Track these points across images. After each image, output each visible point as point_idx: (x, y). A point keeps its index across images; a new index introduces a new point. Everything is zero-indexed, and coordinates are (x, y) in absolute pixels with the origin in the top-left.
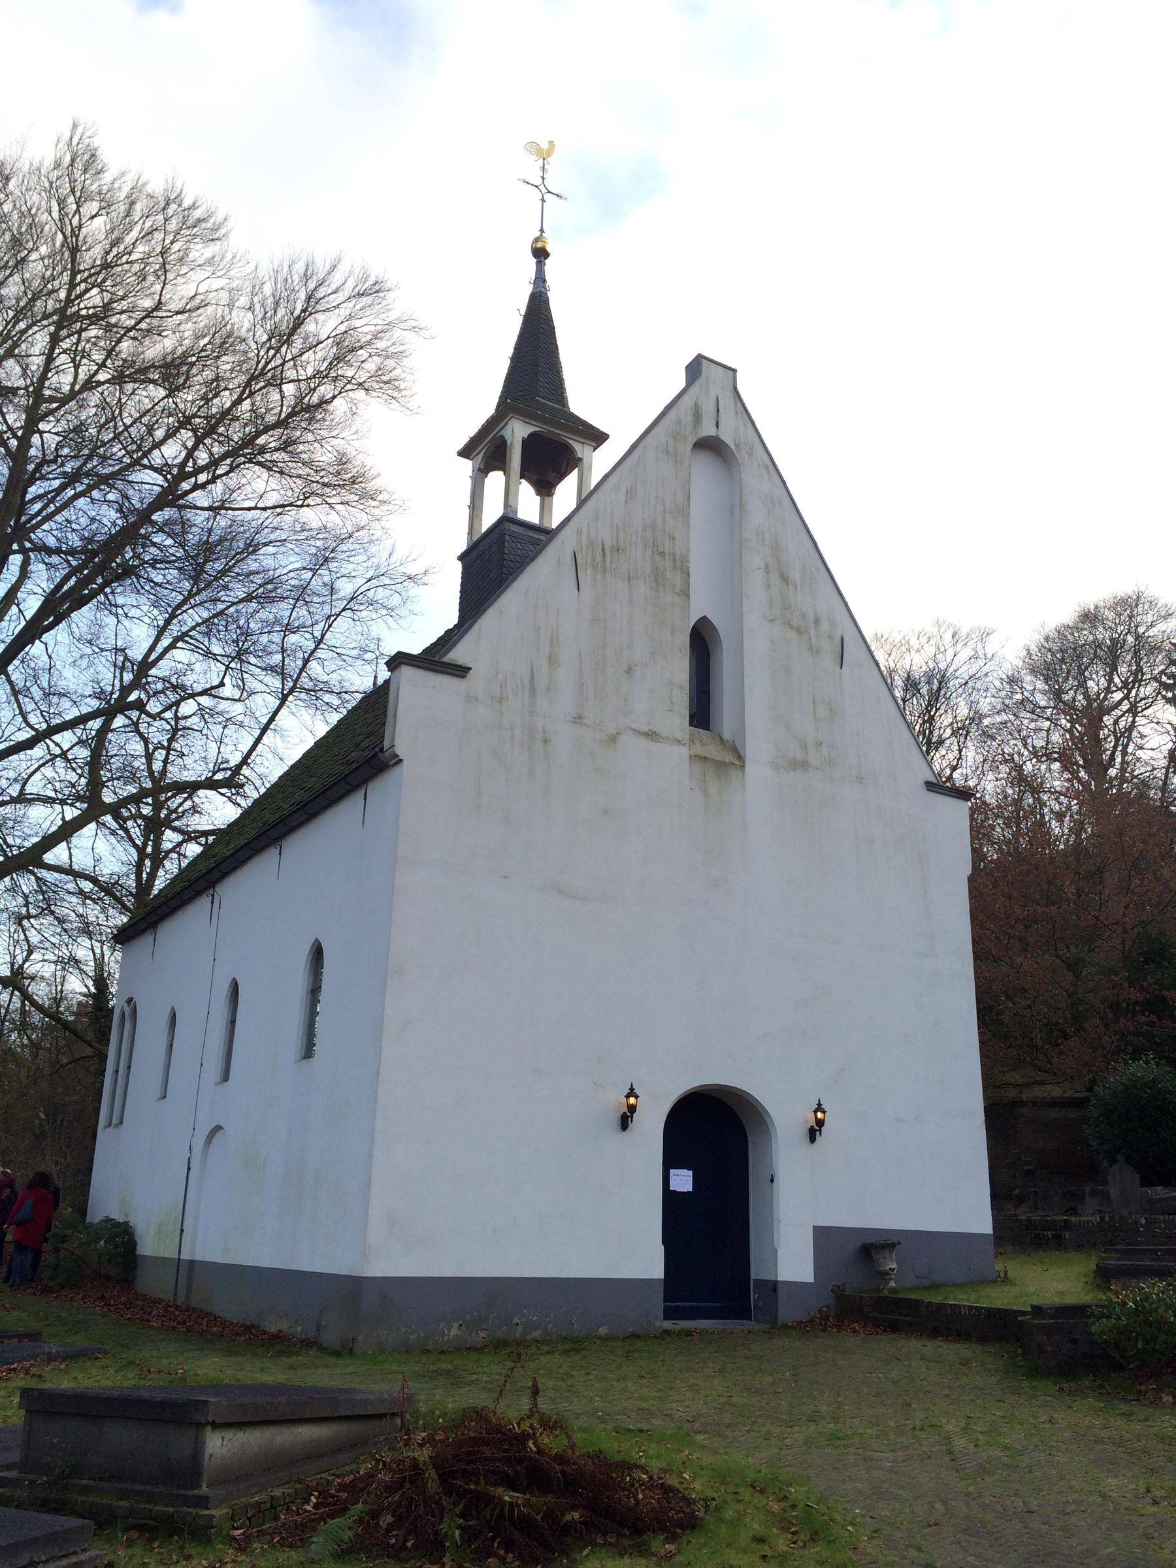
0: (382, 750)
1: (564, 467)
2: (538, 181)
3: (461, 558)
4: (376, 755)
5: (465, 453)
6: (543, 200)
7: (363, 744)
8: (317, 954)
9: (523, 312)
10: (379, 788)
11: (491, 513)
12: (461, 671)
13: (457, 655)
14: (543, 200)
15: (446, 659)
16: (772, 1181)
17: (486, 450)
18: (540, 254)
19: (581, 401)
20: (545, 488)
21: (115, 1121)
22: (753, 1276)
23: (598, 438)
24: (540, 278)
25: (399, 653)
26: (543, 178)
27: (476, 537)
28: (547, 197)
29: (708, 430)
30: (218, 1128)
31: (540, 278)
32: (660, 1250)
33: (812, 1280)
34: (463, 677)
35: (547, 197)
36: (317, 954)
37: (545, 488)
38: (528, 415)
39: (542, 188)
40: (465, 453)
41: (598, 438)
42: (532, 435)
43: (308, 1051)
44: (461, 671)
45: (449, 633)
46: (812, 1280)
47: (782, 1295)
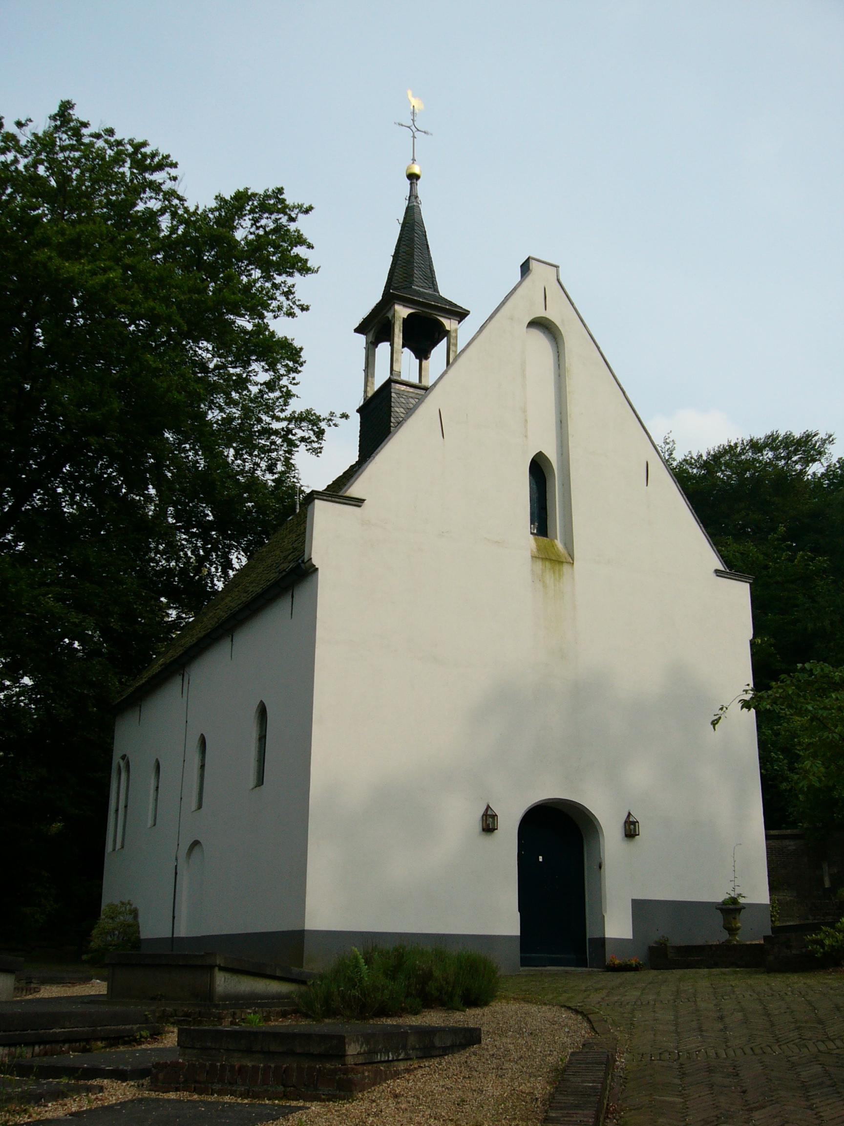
0: (303, 561)
1: (436, 335)
2: (410, 123)
3: (358, 411)
4: (299, 566)
5: (359, 330)
6: (414, 137)
7: (289, 557)
8: (262, 712)
9: (401, 221)
10: (301, 594)
11: (381, 377)
12: (358, 502)
13: (355, 490)
14: (414, 137)
15: (348, 494)
16: (600, 867)
17: (375, 327)
18: (413, 177)
19: (449, 288)
20: (422, 354)
21: (118, 846)
22: (588, 937)
23: (461, 315)
24: (413, 196)
25: (521, 266)
26: (413, 120)
27: (370, 395)
28: (417, 134)
29: (540, 313)
30: (196, 843)
31: (413, 196)
32: (517, 916)
33: (631, 937)
34: (360, 506)
35: (417, 134)
36: (262, 712)
37: (422, 354)
38: (406, 302)
39: (414, 129)
40: (359, 330)
41: (461, 315)
42: (410, 315)
43: (260, 781)
44: (358, 502)
45: (352, 467)
46: (631, 937)
47: (608, 947)
